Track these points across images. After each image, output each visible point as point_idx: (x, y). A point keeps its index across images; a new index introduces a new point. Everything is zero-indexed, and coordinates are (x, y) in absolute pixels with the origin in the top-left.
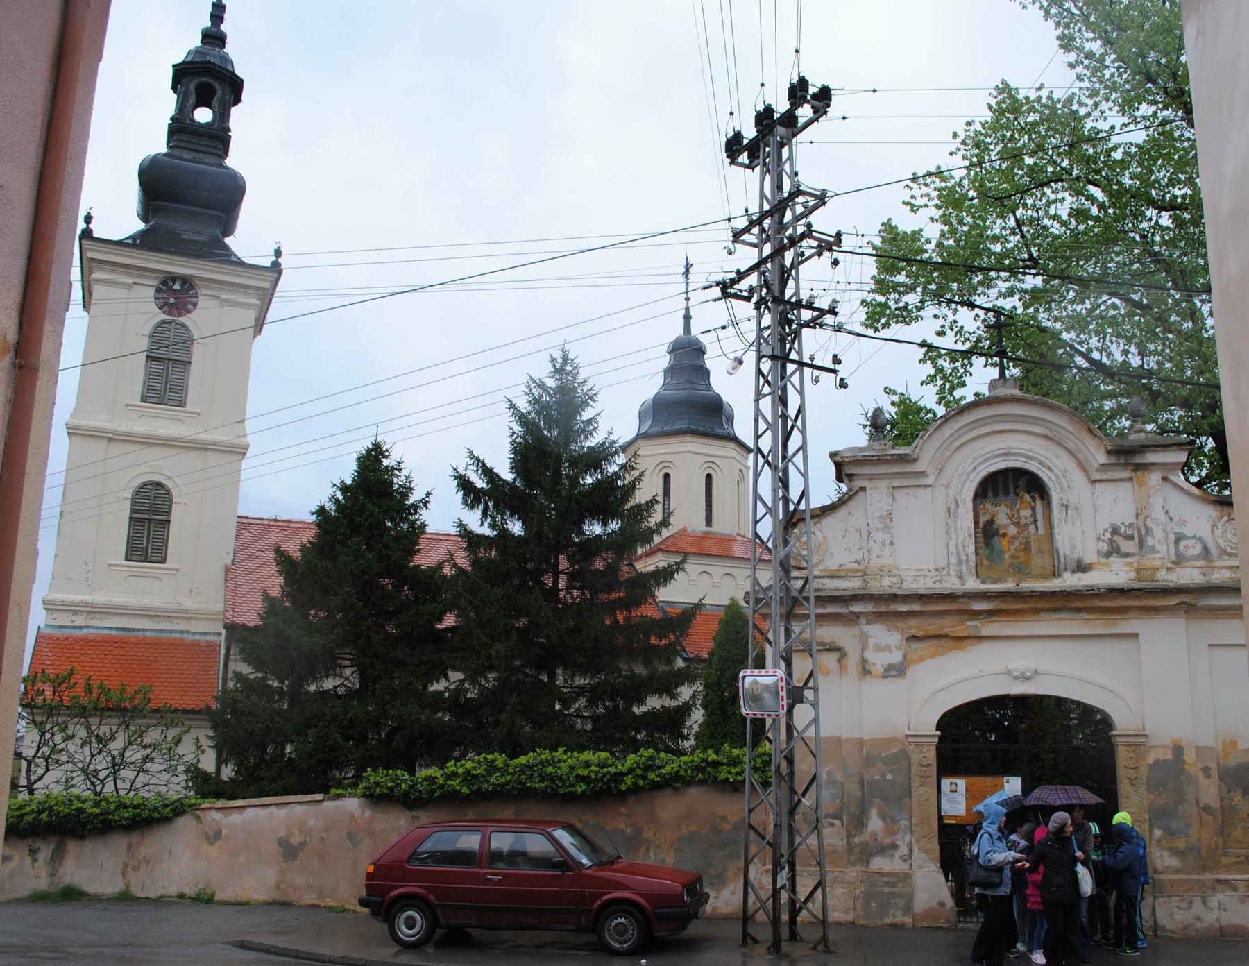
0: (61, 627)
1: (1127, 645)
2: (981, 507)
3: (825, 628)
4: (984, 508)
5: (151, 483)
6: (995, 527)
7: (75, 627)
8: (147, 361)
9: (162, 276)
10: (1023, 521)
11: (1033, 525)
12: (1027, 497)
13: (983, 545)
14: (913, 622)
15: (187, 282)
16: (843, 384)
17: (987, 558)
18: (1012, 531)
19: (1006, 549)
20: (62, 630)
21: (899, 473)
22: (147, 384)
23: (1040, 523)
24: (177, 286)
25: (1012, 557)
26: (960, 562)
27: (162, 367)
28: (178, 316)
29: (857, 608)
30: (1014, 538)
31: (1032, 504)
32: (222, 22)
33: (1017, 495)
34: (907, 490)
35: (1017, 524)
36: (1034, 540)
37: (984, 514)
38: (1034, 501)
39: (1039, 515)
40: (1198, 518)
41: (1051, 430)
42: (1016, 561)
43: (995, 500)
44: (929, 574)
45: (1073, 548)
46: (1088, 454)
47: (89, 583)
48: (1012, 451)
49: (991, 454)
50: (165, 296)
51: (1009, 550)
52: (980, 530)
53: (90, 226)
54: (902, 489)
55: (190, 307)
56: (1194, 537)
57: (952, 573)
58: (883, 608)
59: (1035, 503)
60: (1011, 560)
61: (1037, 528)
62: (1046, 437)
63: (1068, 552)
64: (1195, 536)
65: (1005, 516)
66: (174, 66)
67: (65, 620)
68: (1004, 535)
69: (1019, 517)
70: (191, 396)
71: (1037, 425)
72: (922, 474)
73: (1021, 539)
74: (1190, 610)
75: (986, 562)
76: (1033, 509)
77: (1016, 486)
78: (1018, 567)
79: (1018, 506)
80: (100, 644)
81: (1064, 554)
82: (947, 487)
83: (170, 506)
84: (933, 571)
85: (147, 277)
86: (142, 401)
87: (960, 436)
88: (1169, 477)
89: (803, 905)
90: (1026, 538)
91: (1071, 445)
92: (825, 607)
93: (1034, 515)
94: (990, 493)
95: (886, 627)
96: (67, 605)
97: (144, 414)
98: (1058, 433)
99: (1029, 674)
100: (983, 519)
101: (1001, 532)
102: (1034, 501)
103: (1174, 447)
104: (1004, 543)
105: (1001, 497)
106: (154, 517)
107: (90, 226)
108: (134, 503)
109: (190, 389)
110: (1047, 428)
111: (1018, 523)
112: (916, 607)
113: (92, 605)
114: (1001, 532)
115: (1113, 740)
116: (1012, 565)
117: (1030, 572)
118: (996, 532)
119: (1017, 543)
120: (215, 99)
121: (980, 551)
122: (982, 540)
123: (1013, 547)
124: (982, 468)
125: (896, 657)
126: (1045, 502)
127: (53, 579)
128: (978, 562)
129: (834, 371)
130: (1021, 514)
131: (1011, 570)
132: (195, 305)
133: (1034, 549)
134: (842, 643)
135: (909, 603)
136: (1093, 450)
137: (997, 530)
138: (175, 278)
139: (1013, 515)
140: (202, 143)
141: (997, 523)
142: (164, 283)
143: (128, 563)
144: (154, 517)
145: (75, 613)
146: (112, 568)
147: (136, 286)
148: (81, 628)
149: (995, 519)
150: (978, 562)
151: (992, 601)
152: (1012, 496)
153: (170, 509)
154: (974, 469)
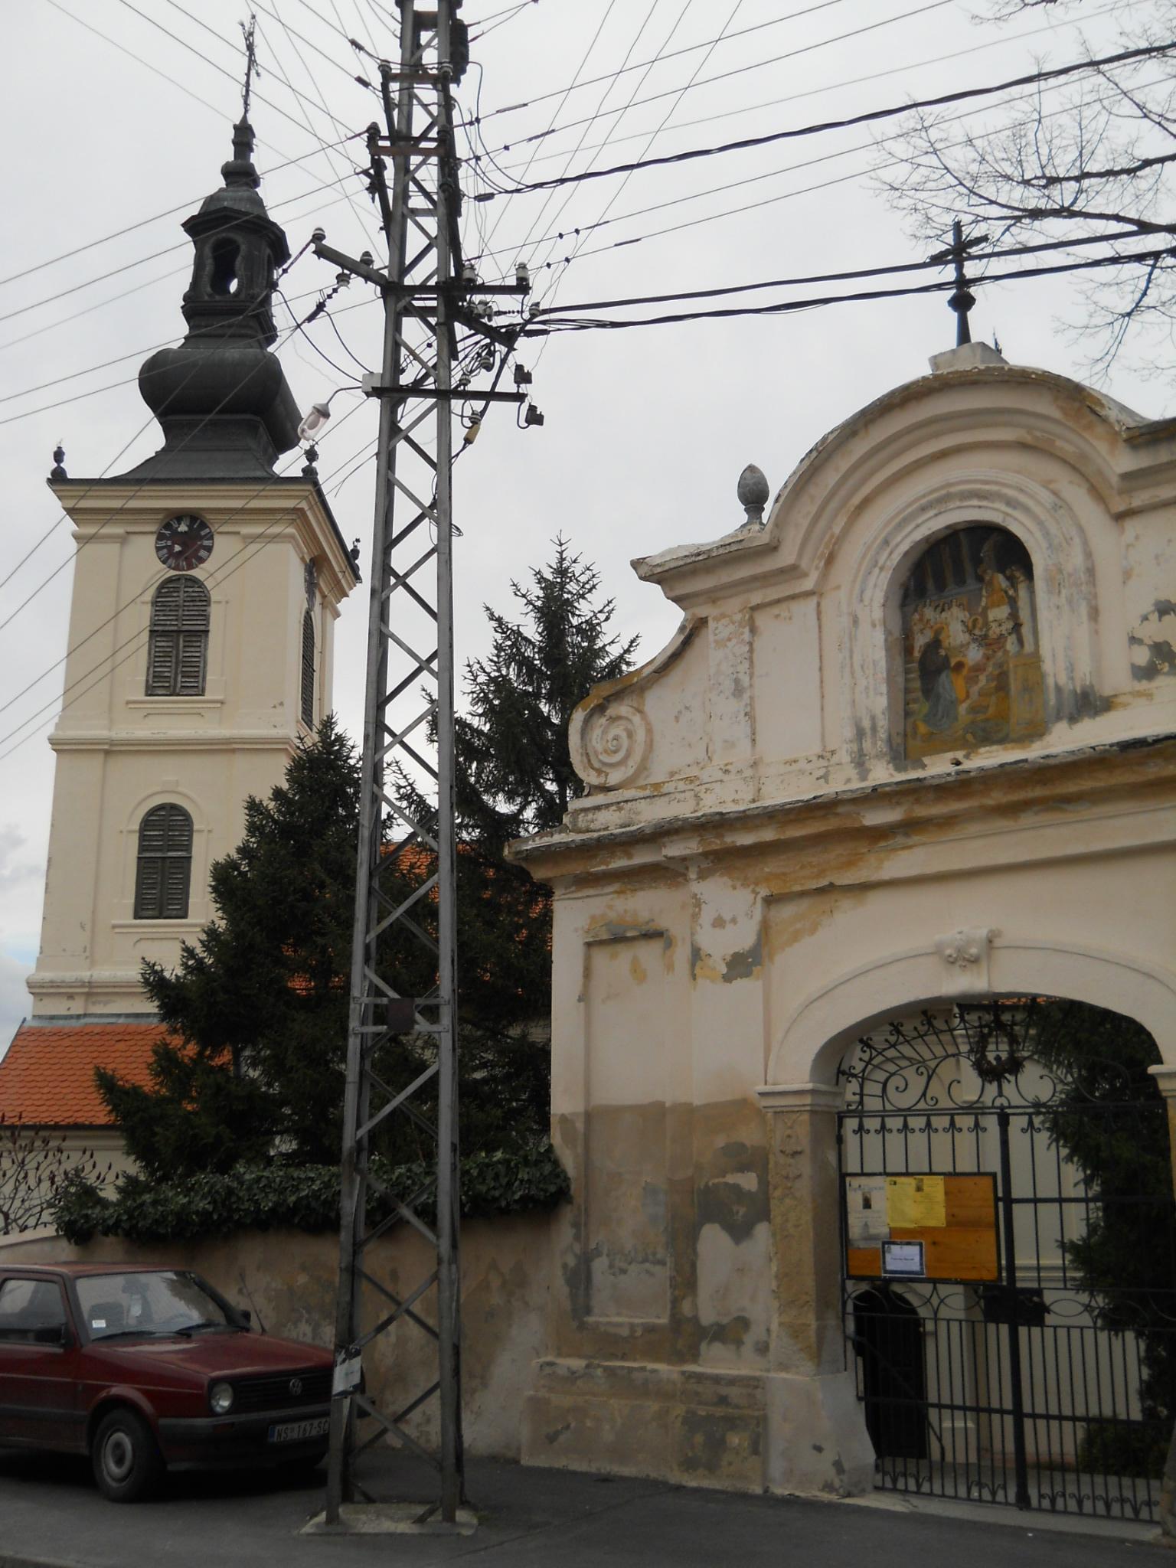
0: (52, 1018)
2: (916, 616)
3: (641, 894)
4: (921, 620)
5: (161, 807)
6: (943, 653)
7: (71, 1017)
8: (151, 637)
9: (160, 516)
10: (995, 631)
11: (1014, 636)
12: (1001, 580)
13: (919, 694)
14: (771, 866)
15: (196, 518)
16: (534, 418)
17: (927, 720)
18: (974, 655)
19: (962, 695)
20: (54, 1021)
21: (754, 578)
22: (151, 669)
24: (183, 528)
25: (973, 710)
27: (170, 644)
28: (188, 569)
29: (675, 849)
30: (978, 669)
31: (1011, 592)
32: (252, 150)
33: (980, 579)
34: (775, 610)
35: (984, 641)
36: (1016, 666)
37: (922, 631)
40: (1170, 541)
42: (980, 717)
45: (1071, 669)
47: (87, 954)
48: (953, 490)
49: (915, 506)
50: (169, 543)
51: (968, 696)
52: (915, 665)
53: (62, 465)
55: (202, 553)
58: (716, 844)
59: (1016, 591)
61: (1021, 641)
62: (1022, 446)
63: (1063, 680)
65: (960, 627)
66: (183, 225)
67: (59, 1007)
68: (960, 665)
69: (986, 623)
70: (212, 677)
71: (1006, 425)
72: (792, 572)
73: (990, 669)
75: (923, 728)
77: (977, 561)
79: (983, 603)
80: (97, 1037)
83: (190, 836)
85: (145, 522)
86: (147, 695)
87: (864, 481)
90: (1001, 665)
92: (630, 856)
94: (930, 585)
95: (730, 883)
96: (58, 987)
97: (150, 711)
99: (974, 951)
100: (920, 641)
101: (953, 662)
106: (170, 854)
107: (62, 465)
108: (143, 838)
109: (210, 668)
111: (986, 636)
112: (768, 835)
113: (90, 984)
114: (953, 662)
115: (1156, 1086)
117: (1007, 735)
118: (944, 665)
119: (983, 679)
120: (239, 260)
121: (914, 707)
122: (917, 684)
123: (975, 690)
124: (899, 539)
125: (743, 936)
127: (41, 953)
128: (909, 730)
129: (519, 397)
132: (209, 549)
134: (663, 923)
135: (756, 828)
137: (947, 658)
138: (179, 515)
139: (975, 621)
140: (203, 324)
141: (945, 644)
142: (167, 526)
143: (138, 921)
144: (170, 854)
145: (71, 996)
146: (117, 930)
147: (133, 538)
148: (79, 1017)
149: (941, 637)
150: (909, 730)
151: (898, 803)
152: (972, 584)
153: (190, 840)
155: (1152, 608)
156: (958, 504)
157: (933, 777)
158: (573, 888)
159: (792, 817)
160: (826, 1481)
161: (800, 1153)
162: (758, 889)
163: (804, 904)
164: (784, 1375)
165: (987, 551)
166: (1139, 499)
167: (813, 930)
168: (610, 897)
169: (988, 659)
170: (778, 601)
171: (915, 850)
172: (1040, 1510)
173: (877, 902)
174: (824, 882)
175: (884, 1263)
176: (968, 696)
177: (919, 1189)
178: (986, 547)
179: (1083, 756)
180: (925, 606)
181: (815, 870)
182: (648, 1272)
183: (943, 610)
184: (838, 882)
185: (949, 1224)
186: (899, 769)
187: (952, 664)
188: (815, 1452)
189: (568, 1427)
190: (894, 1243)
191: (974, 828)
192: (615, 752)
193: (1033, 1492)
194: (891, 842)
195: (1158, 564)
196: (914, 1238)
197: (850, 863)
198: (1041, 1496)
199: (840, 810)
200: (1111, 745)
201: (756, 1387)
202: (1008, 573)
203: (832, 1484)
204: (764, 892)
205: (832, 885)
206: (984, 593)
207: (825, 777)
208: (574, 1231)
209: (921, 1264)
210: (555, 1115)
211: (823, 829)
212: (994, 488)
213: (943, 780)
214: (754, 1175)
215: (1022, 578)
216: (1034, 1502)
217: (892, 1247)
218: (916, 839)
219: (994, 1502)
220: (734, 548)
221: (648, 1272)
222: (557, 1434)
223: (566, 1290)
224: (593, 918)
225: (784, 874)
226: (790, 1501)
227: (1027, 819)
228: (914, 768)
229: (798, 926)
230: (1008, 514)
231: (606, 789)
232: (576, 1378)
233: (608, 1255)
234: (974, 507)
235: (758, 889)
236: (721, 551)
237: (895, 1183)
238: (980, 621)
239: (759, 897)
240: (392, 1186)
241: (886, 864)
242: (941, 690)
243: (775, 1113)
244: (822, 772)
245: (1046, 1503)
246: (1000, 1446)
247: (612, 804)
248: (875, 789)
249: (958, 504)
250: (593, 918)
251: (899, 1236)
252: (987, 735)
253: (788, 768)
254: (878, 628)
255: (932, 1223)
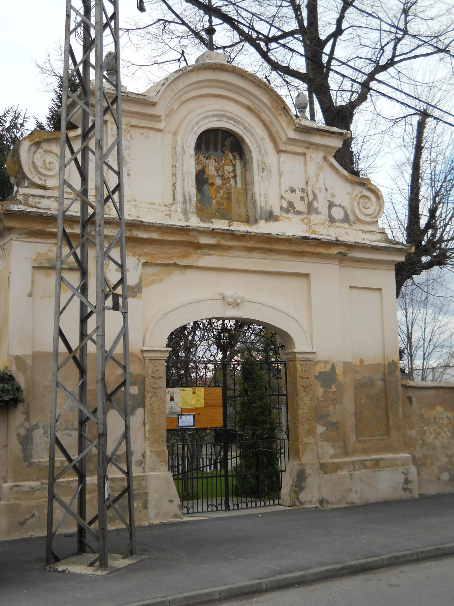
1: (301, 283)
10: (226, 175)
11: (234, 179)
12: (230, 155)
14: (147, 249)
18: (218, 182)
19: (214, 197)
21: (138, 113)
23: (238, 178)
25: (218, 203)
26: (185, 202)
30: (219, 188)
33: (223, 152)
34: (141, 131)
35: (222, 177)
38: (235, 160)
39: (238, 172)
41: (254, 103)
42: (221, 207)
43: (207, 153)
44: (160, 208)
46: (279, 128)
48: (226, 114)
54: (137, 129)
56: (340, 206)
57: (179, 210)
59: (235, 162)
60: (217, 206)
63: (263, 204)
64: (340, 205)
65: (213, 169)
68: (212, 184)
69: (223, 171)
72: (156, 118)
73: (224, 189)
74: (342, 258)
76: (234, 166)
77: (223, 145)
78: (223, 213)
79: (223, 162)
81: (261, 205)
82: (175, 134)
84: (163, 206)
88: (328, 157)
89: (112, 504)
90: (229, 189)
91: (266, 119)
93: (234, 171)
98: (258, 107)
102: (235, 160)
103: (337, 136)
104: (213, 190)
105: (211, 151)
110: (251, 101)
112: (155, 236)
114: (210, 181)
116: (218, 210)
119: (221, 192)
123: (219, 195)
126: (243, 162)
130: (225, 169)
131: (217, 213)
133: (233, 200)
135: (150, 231)
136: (284, 125)
137: (207, 180)
139: (219, 168)
141: (207, 173)
149: (206, 169)
152: (219, 153)
154: (197, 123)
155: (289, 189)
156: (226, 120)
157: (237, 231)
158: (24, 236)
159: (169, 231)
160: (175, 514)
161: (161, 377)
162: (140, 258)
163: (157, 269)
164: (153, 473)
165: (228, 142)
166: (289, 148)
167: (161, 281)
168: (51, 245)
169: (224, 185)
170: (143, 127)
171: (213, 256)
172: (233, 510)
173: (190, 274)
174: (172, 262)
175: (178, 423)
176: (216, 198)
177: (194, 393)
178: (228, 140)
179: (288, 238)
180: (200, 154)
181: (168, 256)
182: (68, 434)
183: (207, 159)
184: (178, 263)
185: (206, 406)
186: (202, 220)
187: (210, 182)
188: (170, 503)
189: (33, 516)
190: (183, 415)
191: (235, 253)
192: (49, 170)
193: (231, 504)
194: (202, 251)
195: (291, 173)
196: (191, 412)
197: (184, 256)
198: (234, 505)
199: (192, 233)
200: (298, 237)
201: (142, 480)
202: (233, 154)
203: (177, 514)
204: (143, 260)
205: (175, 263)
206: (224, 158)
207: (169, 215)
208: (25, 416)
209: (194, 423)
210: (421, 360)
211: (181, 239)
212: (242, 121)
213: (241, 233)
214: (137, 387)
215: (238, 158)
216: (231, 508)
217: (182, 416)
218: (212, 252)
219: (217, 510)
220: (141, 97)
221: (68, 434)
222: (26, 520)
223: (20, 447)
224: (39, 254)
225: (153, 254)
226: (162, 525)
227: (255, 254)
228: (208, 222)
229: (154, 278)
230: (244, 132)
231: (43, 188)
232: (35, 491)
233: (43, 428)
234: (232, 124)
235: (140, 258)
236: (134, 96)
237: (184, 391)
238: (221, 169)
239: (141, 263)
240: (255, 387)
241: (200, 260)
242: (205, 192)
243: (149, 360)
244: (168, 213)
245: (235, 507)
246: (206, 490)
247: (52, 197)
248: (213, 229)
249: (226, 120)
250: (39, 254)
251: (184, 412)
252: (223, 215)
253: (149, 206)
254: (192, 158)
255: (199, 406)
